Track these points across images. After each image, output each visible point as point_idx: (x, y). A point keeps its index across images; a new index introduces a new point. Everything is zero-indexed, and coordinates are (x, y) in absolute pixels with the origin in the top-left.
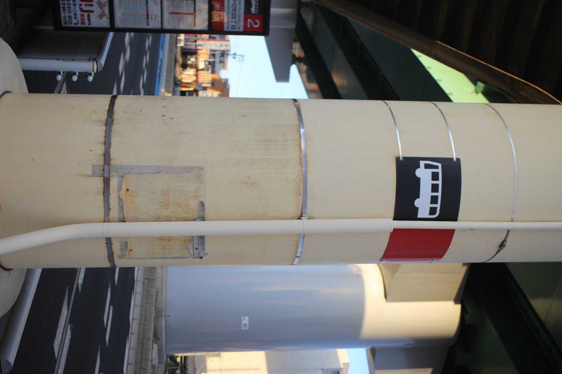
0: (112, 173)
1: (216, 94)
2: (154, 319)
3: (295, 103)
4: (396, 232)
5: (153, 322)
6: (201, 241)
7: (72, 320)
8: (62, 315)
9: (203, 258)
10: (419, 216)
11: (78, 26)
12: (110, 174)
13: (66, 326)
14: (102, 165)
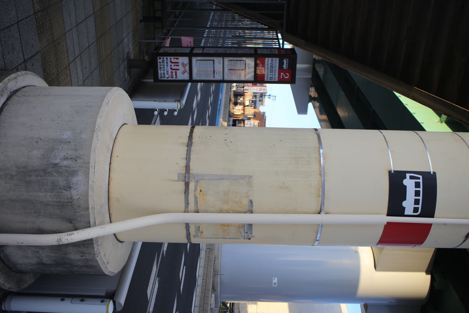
0: (190, 179)
1: (256, 122)
2: (213, 276)
3: (316, 132)
4: (389, 226)
5: (212, 279)
6: (250, 227)
7: (159, 275)
8: (153, 272)
9: (251, 239)
10: (405, 214)
11: (169, 79)
12: (189, 180)
13: (155, 279)
14: (184, 174)
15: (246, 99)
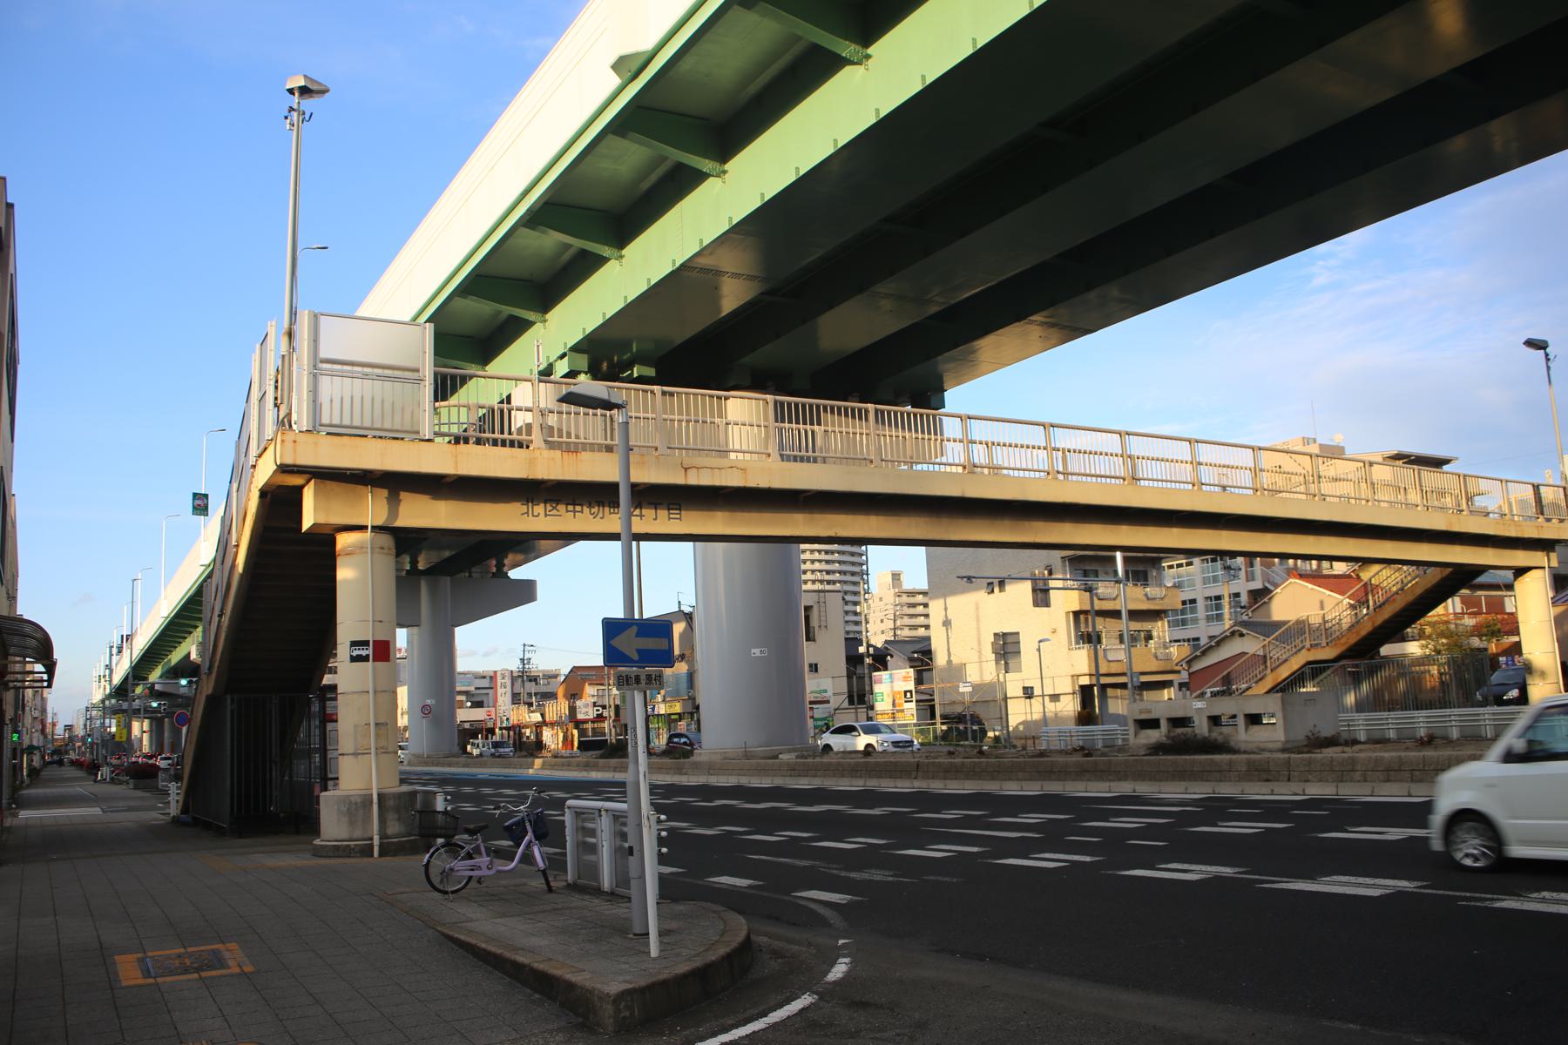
15: (528, 720)
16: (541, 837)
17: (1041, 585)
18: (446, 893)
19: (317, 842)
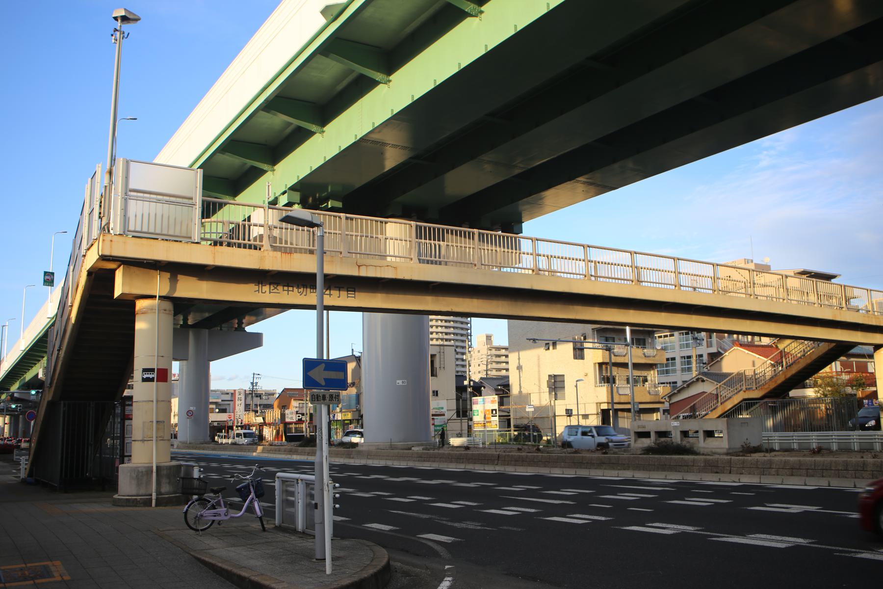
15: (255, 421)
16: (259, 496)
17: (579, 346)
18: (197, 530)
19: (116, 496)
